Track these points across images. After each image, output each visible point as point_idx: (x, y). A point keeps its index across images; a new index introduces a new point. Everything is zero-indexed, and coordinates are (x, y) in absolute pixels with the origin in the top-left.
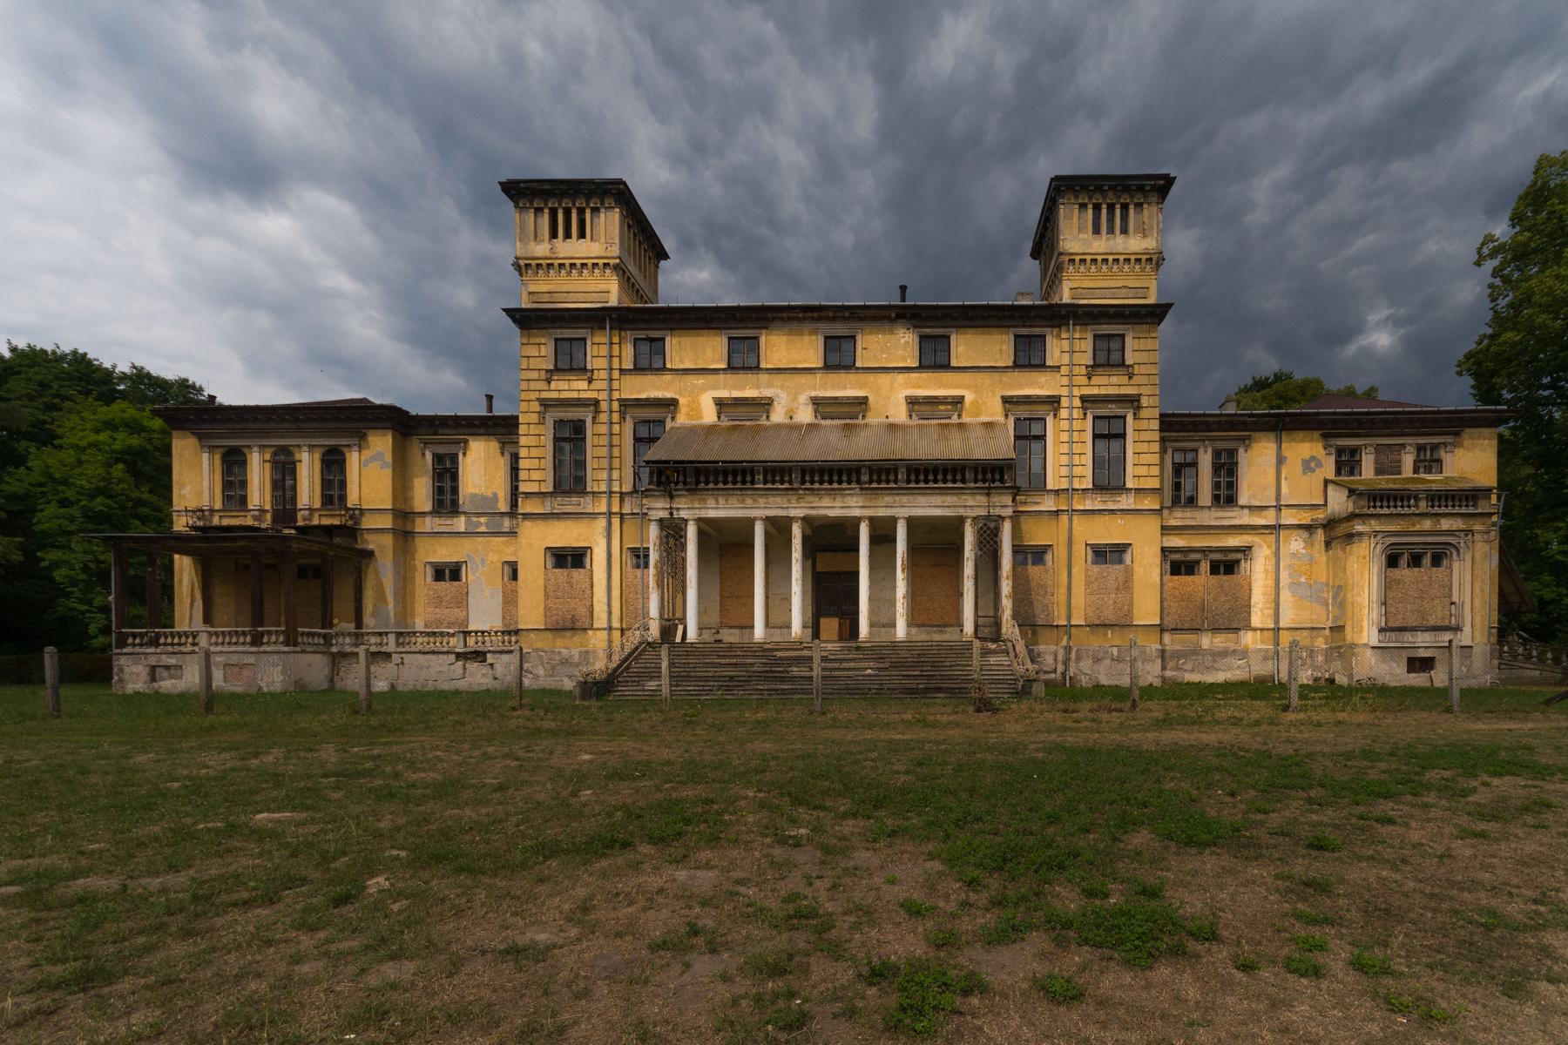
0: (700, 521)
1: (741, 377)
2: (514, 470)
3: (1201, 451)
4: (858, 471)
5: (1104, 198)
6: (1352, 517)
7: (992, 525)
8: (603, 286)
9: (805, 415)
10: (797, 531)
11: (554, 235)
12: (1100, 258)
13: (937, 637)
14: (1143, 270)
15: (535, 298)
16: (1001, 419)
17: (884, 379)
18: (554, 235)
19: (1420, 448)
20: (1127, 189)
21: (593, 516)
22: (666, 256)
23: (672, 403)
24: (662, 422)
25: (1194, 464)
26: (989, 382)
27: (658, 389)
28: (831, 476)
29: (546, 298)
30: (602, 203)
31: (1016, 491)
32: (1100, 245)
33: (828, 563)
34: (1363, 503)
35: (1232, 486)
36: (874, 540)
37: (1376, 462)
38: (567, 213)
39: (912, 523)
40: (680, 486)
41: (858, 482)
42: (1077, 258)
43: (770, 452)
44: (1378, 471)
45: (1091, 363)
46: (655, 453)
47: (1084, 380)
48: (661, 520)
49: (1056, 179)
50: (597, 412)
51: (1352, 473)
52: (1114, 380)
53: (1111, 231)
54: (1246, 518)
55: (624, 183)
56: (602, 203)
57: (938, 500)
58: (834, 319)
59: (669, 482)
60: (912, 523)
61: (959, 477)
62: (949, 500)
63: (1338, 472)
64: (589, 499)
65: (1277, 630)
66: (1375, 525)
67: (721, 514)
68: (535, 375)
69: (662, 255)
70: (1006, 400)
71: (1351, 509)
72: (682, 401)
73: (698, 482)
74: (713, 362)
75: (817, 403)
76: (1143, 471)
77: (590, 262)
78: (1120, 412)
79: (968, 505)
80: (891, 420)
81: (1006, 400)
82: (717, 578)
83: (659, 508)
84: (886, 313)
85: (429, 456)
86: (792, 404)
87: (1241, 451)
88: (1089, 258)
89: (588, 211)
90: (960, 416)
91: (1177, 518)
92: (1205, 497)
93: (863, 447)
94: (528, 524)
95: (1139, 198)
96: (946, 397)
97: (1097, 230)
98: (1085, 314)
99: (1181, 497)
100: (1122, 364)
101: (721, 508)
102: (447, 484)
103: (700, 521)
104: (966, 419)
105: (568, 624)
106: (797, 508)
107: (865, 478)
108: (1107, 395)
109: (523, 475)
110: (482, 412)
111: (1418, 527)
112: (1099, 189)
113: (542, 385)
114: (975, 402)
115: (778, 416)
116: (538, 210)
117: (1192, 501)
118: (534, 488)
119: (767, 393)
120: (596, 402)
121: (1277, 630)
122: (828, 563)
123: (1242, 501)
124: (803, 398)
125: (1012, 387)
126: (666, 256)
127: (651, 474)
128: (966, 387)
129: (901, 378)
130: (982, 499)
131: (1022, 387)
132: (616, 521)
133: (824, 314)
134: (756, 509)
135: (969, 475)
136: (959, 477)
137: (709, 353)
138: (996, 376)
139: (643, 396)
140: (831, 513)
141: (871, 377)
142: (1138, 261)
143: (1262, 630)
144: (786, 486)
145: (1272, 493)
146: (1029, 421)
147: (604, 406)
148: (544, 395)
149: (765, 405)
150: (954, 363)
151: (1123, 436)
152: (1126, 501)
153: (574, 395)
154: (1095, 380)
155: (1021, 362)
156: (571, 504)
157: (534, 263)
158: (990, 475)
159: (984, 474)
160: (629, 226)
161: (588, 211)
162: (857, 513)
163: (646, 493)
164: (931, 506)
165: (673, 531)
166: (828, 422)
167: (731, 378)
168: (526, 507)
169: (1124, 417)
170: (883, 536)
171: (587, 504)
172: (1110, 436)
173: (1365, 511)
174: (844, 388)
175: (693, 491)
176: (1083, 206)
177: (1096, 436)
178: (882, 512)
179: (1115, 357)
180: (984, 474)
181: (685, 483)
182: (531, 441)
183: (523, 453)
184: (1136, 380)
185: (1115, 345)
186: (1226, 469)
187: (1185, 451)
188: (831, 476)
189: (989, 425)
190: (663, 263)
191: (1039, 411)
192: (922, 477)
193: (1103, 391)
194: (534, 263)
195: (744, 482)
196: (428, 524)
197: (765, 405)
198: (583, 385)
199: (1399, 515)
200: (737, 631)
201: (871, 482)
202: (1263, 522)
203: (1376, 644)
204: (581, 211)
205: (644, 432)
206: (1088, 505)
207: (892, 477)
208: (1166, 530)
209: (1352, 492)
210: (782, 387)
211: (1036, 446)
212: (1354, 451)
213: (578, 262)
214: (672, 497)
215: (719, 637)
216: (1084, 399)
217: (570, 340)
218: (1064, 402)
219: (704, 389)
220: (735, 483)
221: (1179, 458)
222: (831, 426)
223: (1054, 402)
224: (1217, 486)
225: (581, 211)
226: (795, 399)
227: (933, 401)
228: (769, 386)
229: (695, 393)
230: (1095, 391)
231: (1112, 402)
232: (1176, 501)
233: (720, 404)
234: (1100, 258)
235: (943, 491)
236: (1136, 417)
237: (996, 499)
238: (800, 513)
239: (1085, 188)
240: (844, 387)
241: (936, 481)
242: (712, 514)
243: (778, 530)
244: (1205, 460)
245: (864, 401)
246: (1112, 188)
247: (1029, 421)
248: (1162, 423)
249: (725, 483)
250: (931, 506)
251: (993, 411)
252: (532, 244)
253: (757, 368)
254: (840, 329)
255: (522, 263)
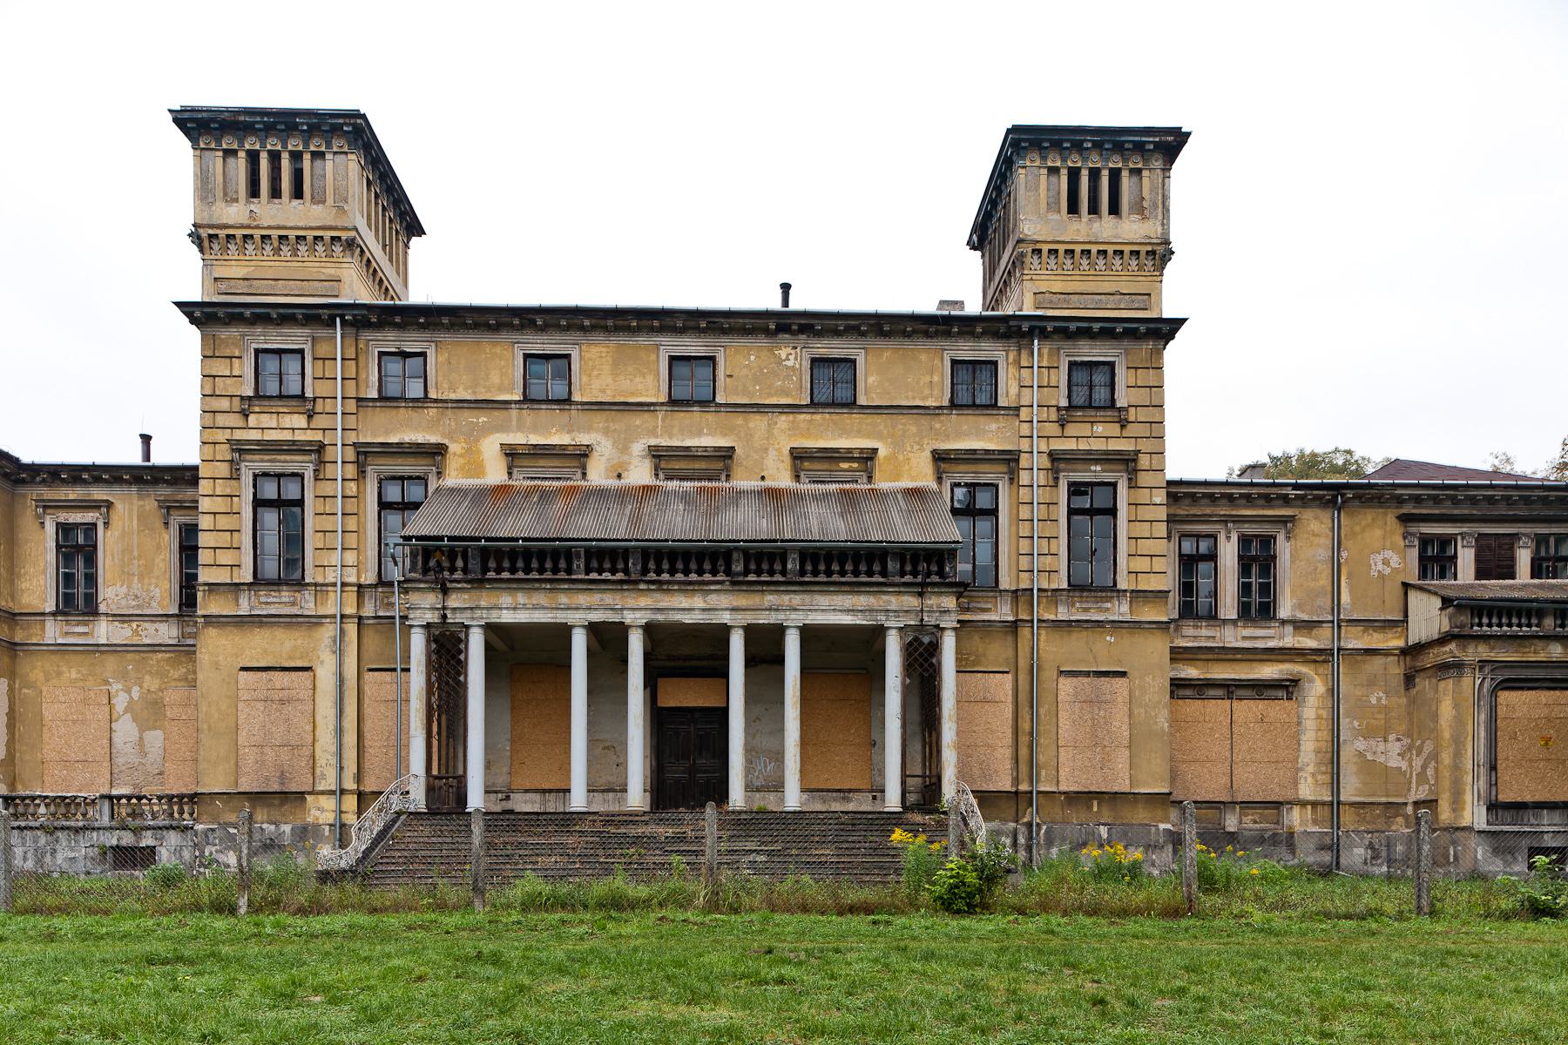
0: (491, 629)
1: (545, 414)
2: (188, 550)
3: (1222, 538)
4: (783, 556)
5: (1085, 160)
6: (1444, 640)
7: (926, 640)
8: (330, 272)
9: (640, 474)
10: (636, 645)
11: (254, 192)
12: (1078, 248)
13: (837, 806)
14: (1141, 267)
15: (223, 287)
16: (932, 484)
17: (758, 422)
18: (254, 192)
19: (1541, 540)
20: (1119, 148)
21: (315, 621)
22: (420, 232)
23: (436, 453)
24: (422, 480)
25: (1212, 557)
26: (914, 429)
27: (416, 429)
28: (686, 564)
29: (242, 287)
30: (329, 145)
31: (961, 589)
32: (1082, 229)
33: (684, 695)
34: (1465, 618)
35: (1268, 590)
36: (750, 662)
37: (1478, 559)
38: (275, 157)
39: (809, 635)
40: (458, 575)
41: (728, 572)
42: (1045, 248)
43: (588, 526)
44: (1480, 574)
45: (1064, 403)
46: (422, 524)
47: (1054, 429)
48: (428, 626)
49: (1014, 130)
50: (321, 462)
51: (1442, 576)
52: (1099, 429)
53: (1094, 209)
54: (1290, 639)
55: (364, 117)
56: (329, 145)
57: (847, 601)
58: (681, 331)
59: (440, 568)
60: (809, 635)
61: (877, 567)
62: (862, 601)
63: (1423, 574)
64: (308, 595)
65: (1335, 806)
66: (1482, 652)
67: (522, 617)
68: (224, 404)
69: (414, 228)
70: (940, 457)
71: (1446, 627)
72: (454, 448)
73: (485, 570)
74: (501, 389)
75: (659, 456)
76: (1142, 564)
77: (310, 234)
78: (1108, 477)
79: (891, 610)
80: (768, 483)
81: (940, 457)
82: (507, 717)
83: (424, 606)
84: (482, 319)
85: (50, 528)
86: (619, 459)
87: (1281, 538)
88: (1062, 248)
89: (307, 157)
90: (870, 479)
91: (1196, 635)
92: (1229, 606)
93: (745, 523)
94: (212, 632)
95: (1136, 162)
96: (849, 450)
97: (1073, 208)
98: (1057, 330)
99: (1193, 605)
100: (1112, 404)
101: (519, 608)
102: (80, 568)
103: (491, 629)
104: (882, 484)
105: (276, 787)
106: (637, 609)
107: (738, 567)
108: (1089, 452)
109: (204, 557)
110: (135, 459)
111: (1541, 657)
112: (1078, 147)
113: (235, 420)
114: (892, 457)
115: (597, 475)
116: (229, 153)
117: (1212, 616)
118: (222, 576)
119: (584, 439)
120: (320, 448)
121: (1335, 806)
122: (684, 695)
123: (1284, 612)
124: (638, 448)
125: (947, 437)
126: (420, 232)
127: (414, 555)
128: (879, 436)
129: (783, 421)
130: (911, 601)
131: (960, 435)
132: (352, 629)
133: (668, 321)
134: (576, 610)
135: (892, 566)
136: (877, 567)
137: (495, 378)
138: (925, 421)
139: (394, 439)
140: (687, 619)
141: (739, 420)
142: (1136, 253)
143: (1314, 804)
144: (620, 576)
145: (1326, 602)
146: (975, 491)
147: (336, 453)
148: (239, 435)
149: (580, 456)
150: (862, 401)
151: (1112, 512)
152: (1120, 610)
153: (287, 436)
154: (1072, 429)
155: (964, 398)
156: (279, 602)
157: (222, 233)
158: (924, 566)
159: (915, 564)
160: (369, 183)
161: (307, 157)
162: (726, 618)
163: (405, 586)
164: (836, 609)
165: (446, 649)
166: (673, 485)
167: (528, 416)
168: (208, 606)
169: (1114, 485)
170: (765, 649)
171: (308, 604)
172: (1091, 512)
173: (1467, 631)
174: (700, 434)
175: (479, 583)
176: (1054, 171)
177: (1072, 512)
178: (764, 619)
179: (1101, 395)
180: (915, 564)
181: (465, 570)
182: (220, 505)
183: (205, 522)
184: (1132, 430)
185: (1100, 378)
186: (1258, 560)
187: (1198, 537)
188: (686, 564)
189: (915, 494)
190: (414, 239)
191: (988, 474)
192: (849, 567)
193: (1083, 446)
194: (222, 233)
195: (555, 570)
196: (53, 632)
197: (580, 456)
198: (301, 421)
199: (1515, 637)
200: (536, 797)
201: (746, 572)
202: (1310, 643)
203: (1483, 826)
204: (296, 156)
205: (393, 493)
206: (1063, 613)
207: (778, 567)
208: (1179, 655)
209: (1446, 602)
210: (606, 432)
211: (984, 525)
212: (1445, 541)
213: (292, 234)
214: (445, 591)
215: (509, 805)
216: (1054, 456)
217: (280, 352)
218: (1024, 463)
219: (487, 430)
220: (541, 570)
221: (1188, 547)
222: (685, 497)
223: (1010, 460)
224: (1245, 589)
225: (296, 156)
226: (625, 449)
227: (831, 456)
228: (589, 429)
229: (474, 436)
230: (1070, 445)
231: (1097, 461)
232: (1188, 611)
233: (512, 455)
234: (1078, 248)
235: (855, 588)
236: (1133, 485)
237: (932, 601)
238: (794, 620)
239: (1057, 145)
240: (700, 433)
241: (843, 573)
242: (507, 617)
243: (608, 642)
244: (1229, 552)
245: (726, 454)
246: (1098, 146)
247: (975, 491)
248: (1169, 494)
249: (527, 571)
250: (836, 609)
251: (921, 474)
252: (220, 204)
253: (567, 401)
254: (691, 346)
255: (204, 233)
